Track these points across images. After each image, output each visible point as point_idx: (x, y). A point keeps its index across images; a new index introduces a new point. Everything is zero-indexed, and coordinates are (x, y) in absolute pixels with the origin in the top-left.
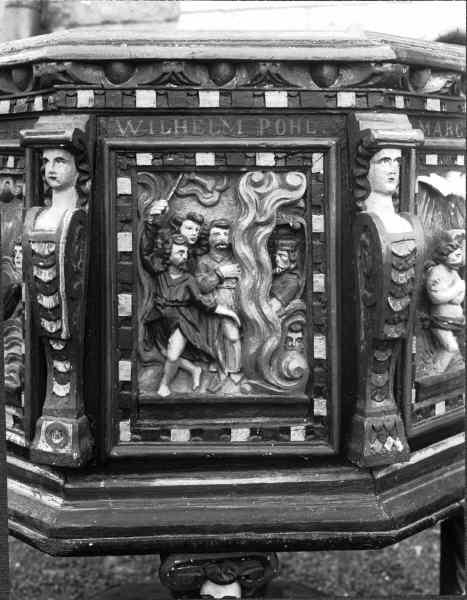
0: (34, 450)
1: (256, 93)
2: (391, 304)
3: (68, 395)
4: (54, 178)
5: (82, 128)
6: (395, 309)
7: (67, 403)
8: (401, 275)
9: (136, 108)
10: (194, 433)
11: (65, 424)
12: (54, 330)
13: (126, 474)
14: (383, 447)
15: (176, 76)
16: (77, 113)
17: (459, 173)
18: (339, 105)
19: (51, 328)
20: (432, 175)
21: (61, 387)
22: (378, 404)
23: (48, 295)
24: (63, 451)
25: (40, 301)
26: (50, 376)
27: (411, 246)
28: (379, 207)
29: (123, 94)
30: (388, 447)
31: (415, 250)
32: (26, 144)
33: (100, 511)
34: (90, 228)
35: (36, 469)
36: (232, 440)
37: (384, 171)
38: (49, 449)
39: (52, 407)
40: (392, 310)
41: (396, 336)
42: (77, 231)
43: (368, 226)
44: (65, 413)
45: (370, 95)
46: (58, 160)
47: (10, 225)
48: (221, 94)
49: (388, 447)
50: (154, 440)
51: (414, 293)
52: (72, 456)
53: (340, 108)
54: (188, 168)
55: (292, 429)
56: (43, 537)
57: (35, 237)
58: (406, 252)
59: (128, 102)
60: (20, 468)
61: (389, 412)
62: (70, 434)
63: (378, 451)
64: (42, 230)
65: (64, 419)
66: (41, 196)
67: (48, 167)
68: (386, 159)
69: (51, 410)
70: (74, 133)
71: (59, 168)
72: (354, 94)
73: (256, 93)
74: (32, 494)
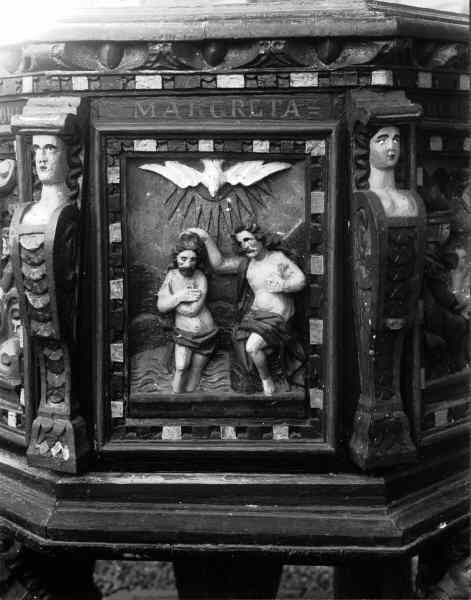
2: (30, 299)
5: (74, 111)
6: (35, 306)
8: (35, 270)
10: (185, 430)
13: (248, 472)
14: (49, 451)
17: (261, 163)
20: (168, 163)
22: (53, 405)
27: (39, 240)
30: (54, 451)
31: (42, 245)
32: (16, 129)
33: (77, 513)
34: (74, 223)
35: (46, 476)
36: (437, 425)
40: (32, 307)
41: (46, 335)
42: (69, 229)
45: (177, 78)
48: (319, 77)
49: (54, 451)
51: (373, 289)
53: (221, 89)
54: (297, 157)
55: (164, 428)
58: (34, 246)
61: (61, 417)
63: (42, 452)
70: (66, 120)
72: (85, 78)
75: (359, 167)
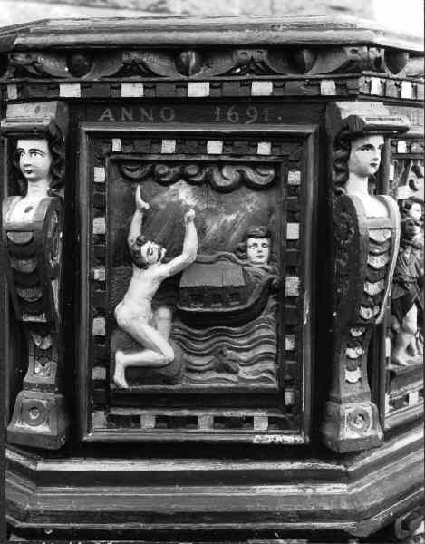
0: (343, 440)
1: (113, 85)
3: (360, 379)
4: (30, 172)
7: (361, 388)
9: (187, 98)
11: (365, 408)
12: (370, 316)
15: (255, 65)
16: (371, 100)
18: (61, 95)
19: (368, 314)
21: (352, 373)
23: (373, 282)
24: (368, 434)
25: (365, 290)
26: (343, 365)
28: (357, 189)
29: (177, 87)
37: (366, 157)
38: (356, 436)
39: (349, 395)
43: (347, 205)
44: (361, 397)
46: (33, 152)
47: (232, 217)
50: (400, 407)
52: (377, 437)
56: (351, 523)
57: (372, 224)
59: (114, 94)
60: (270, 471)
62: (370, 415)
64: (373, 217)
65: (361, 403)
66: (18, 185)
67: (25, 160)
68: (369, 147)
69: (349, 398)
71: (35, 157)
73: (113, 85)
74: (301, 491)
75: (338, 171)
